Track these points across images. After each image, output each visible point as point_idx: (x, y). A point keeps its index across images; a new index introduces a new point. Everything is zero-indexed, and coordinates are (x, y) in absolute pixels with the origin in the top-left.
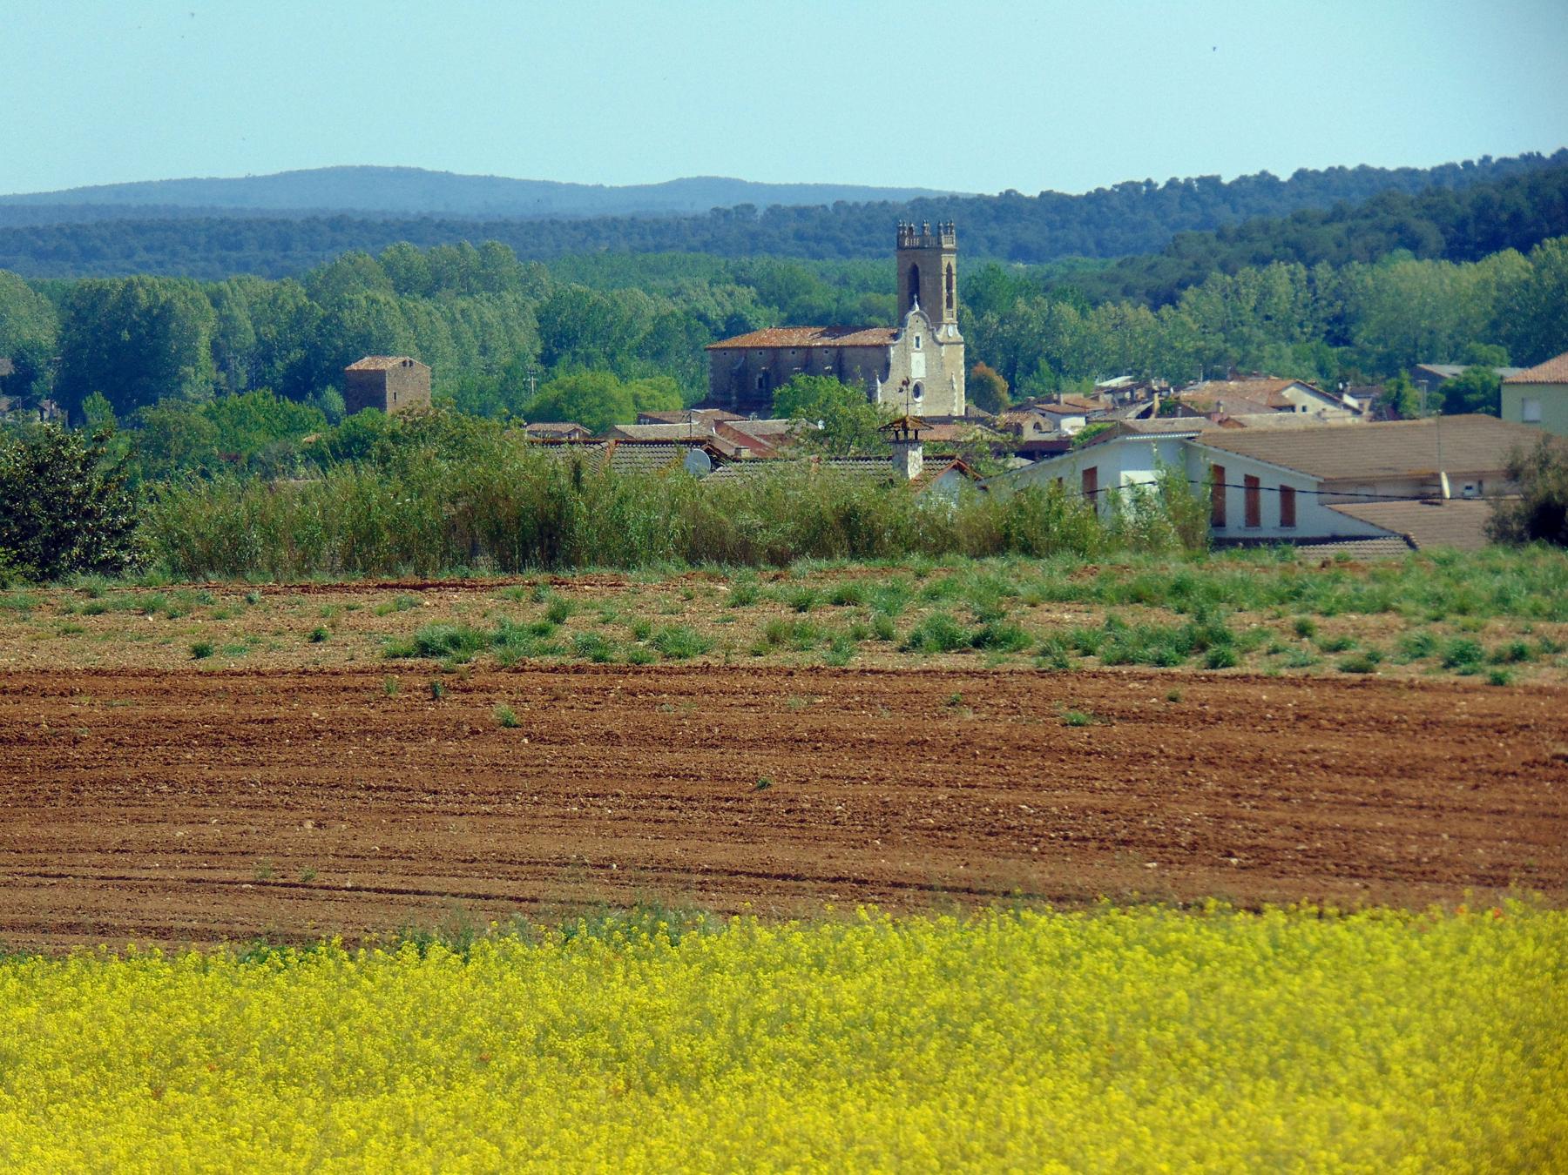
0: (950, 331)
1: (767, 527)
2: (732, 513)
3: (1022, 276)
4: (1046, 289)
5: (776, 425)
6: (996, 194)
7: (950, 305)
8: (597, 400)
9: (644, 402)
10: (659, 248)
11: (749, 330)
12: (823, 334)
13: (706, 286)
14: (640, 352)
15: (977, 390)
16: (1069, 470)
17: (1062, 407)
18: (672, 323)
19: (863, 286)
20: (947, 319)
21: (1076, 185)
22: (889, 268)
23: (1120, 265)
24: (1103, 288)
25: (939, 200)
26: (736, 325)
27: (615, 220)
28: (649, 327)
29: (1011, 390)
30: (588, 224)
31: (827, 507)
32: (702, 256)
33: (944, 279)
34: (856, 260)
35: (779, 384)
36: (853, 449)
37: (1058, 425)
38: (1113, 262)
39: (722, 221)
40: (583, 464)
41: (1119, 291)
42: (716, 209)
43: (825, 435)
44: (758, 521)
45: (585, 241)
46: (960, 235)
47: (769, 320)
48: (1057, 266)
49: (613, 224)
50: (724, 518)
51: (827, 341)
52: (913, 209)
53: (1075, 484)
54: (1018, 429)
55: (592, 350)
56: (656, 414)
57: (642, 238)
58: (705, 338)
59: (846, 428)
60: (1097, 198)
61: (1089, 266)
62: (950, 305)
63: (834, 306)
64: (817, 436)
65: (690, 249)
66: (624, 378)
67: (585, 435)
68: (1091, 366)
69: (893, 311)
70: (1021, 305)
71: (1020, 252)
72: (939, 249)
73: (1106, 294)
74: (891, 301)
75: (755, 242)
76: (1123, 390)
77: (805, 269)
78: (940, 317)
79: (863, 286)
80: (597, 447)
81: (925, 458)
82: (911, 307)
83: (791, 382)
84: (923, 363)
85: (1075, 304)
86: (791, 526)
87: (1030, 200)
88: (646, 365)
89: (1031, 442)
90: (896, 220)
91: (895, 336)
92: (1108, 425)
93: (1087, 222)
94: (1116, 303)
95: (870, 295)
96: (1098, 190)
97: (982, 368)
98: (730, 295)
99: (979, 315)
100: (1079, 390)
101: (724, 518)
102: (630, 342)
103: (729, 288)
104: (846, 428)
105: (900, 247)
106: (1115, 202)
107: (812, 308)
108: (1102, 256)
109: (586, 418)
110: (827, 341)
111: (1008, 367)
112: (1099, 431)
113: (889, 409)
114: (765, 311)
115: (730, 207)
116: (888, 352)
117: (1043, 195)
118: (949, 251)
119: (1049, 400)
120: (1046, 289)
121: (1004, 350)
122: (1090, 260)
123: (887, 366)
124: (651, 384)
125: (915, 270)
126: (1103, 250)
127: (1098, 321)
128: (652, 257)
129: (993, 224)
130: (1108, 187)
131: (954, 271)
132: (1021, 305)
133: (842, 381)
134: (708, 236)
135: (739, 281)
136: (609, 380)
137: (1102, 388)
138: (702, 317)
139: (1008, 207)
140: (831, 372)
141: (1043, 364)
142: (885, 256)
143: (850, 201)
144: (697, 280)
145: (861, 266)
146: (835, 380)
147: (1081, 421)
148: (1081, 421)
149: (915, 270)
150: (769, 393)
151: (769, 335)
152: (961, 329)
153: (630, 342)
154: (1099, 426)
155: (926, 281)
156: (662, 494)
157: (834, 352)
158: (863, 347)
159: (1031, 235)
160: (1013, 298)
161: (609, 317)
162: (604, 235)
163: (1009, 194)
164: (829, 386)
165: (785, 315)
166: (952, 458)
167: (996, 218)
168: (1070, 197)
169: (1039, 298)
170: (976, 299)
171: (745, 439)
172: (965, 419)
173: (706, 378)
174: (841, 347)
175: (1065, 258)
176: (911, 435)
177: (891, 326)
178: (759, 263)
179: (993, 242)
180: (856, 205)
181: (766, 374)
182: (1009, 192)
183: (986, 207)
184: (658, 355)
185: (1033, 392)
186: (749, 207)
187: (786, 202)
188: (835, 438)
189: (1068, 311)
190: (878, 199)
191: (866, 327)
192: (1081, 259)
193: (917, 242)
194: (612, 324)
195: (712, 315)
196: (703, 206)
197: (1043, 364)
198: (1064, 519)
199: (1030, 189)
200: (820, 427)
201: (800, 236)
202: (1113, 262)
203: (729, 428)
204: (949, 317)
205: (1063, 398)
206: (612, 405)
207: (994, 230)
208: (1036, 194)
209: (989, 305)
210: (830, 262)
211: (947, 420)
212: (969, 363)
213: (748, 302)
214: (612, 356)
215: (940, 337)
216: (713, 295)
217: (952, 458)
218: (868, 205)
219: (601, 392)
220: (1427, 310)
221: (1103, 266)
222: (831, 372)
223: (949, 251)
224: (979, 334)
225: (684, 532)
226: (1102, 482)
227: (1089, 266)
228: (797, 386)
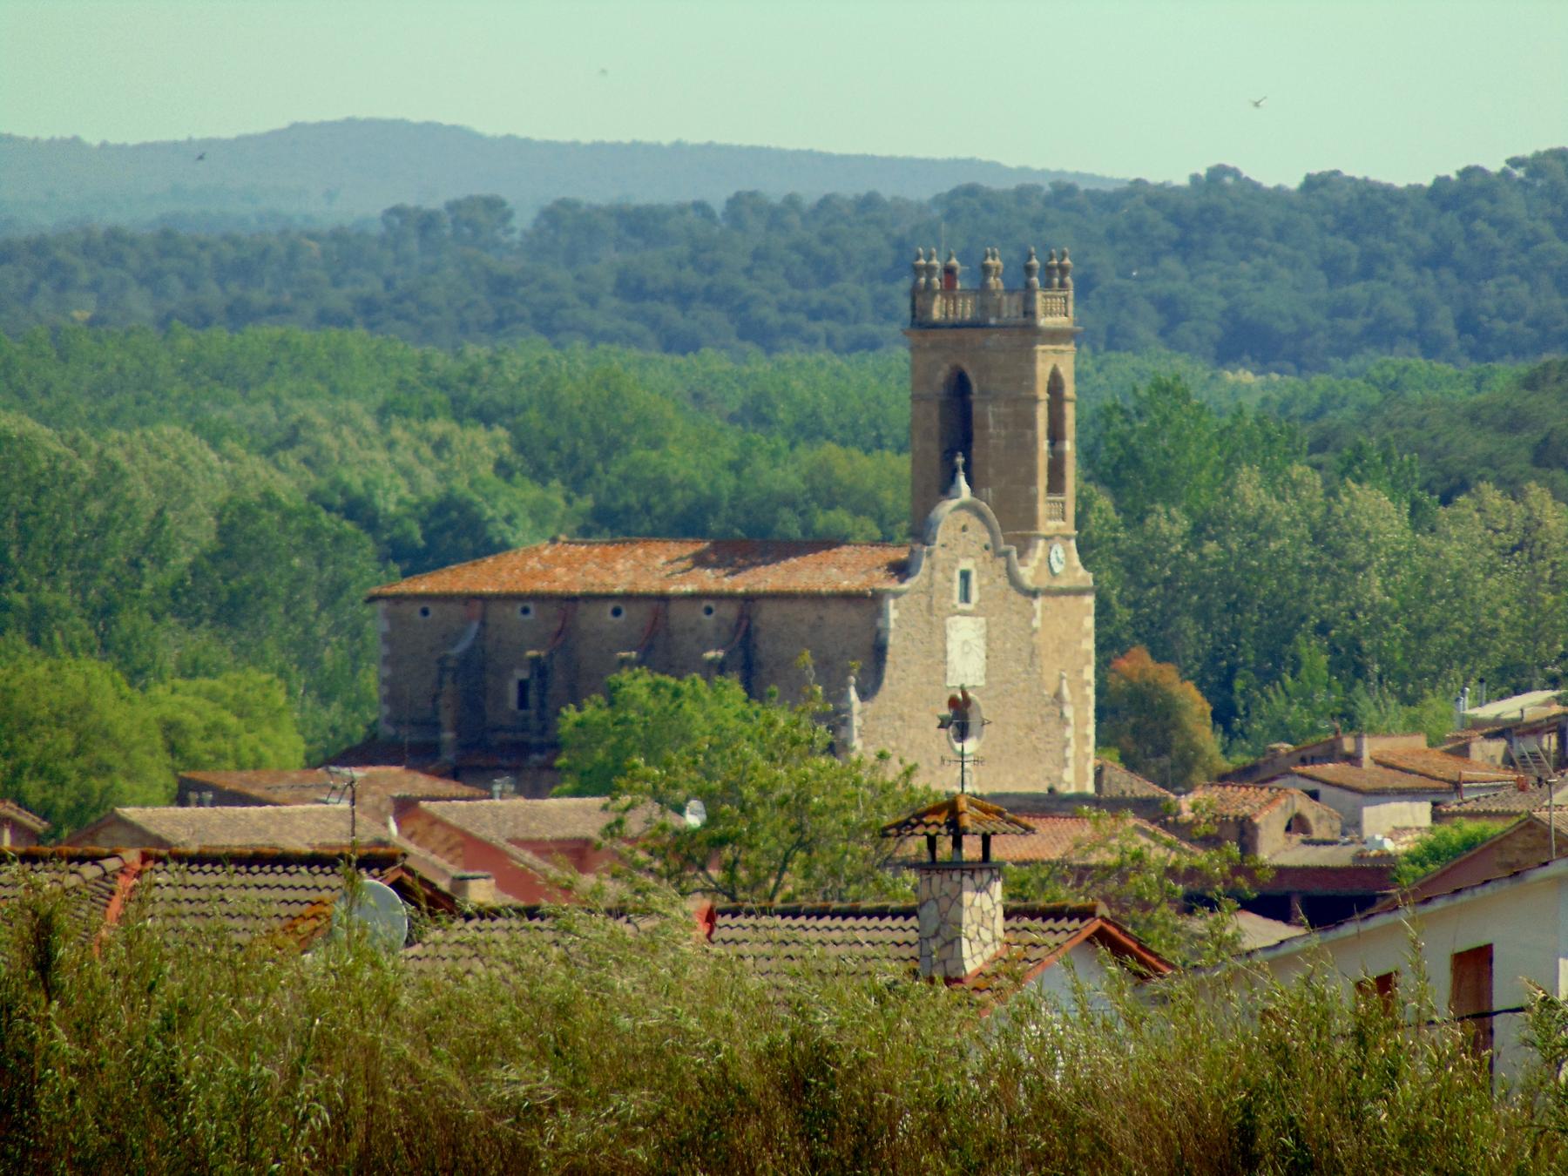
0: (1056, 557)
1: (571, 1102)
2: (473, 1059)
3: (1251, 403)
4: (1319, 446)
5: (571, 814)
6: (1182, 180)
7: (1056, 485)
8: (68, 742)
9: (197, 746)
10: (239, 315)
11: (488, 547)
12: (700, 561)
13: (369, 424)
14: (180, 603)
15: (1131, 723)
16: (1413, 948)
17: (1367, 773)
18: (269, 520)
19: (809, 429)
20: (1048, 526)
21: (1407, 159)
22: (889, 381)
23: (1531, 383)
24: (1480, 444)
25: (1023, 194)
26: (455, 531)
27: (114, 235)
28: (205, 534)
29: (1223, 716)
30: (39, 247)
31: (743, 1051)
32: (357, 340)
33: (1042, 413)
34: (790, 357)
35: (576, 697)
36: (792, 882)
37: (1353, 824)
38: (1505, 374)
39: (413, 245)
40: (63, 920)
41: (1525, 453)
42: (397, 211)
43: (714, 841)
44: (547, 1083)
45: (33, 289)
46: (1085, 287)
47: (540, 515)
48: (1350, 384)
49: (108, 247)
50: (454, 1079)
51: (710, 580)
52: (952, 215)
53: (1430, 989)
54: (1245, 832)
55: (46, 596)
56: (232, 781)
57: (191, 286)
58: (364, 567)
59: (772, 832)
60: (1463, 195)
61: (1441, 384)
62: (1056, 485)
63: (727, 482)
64: (683, 856)
65: (325, 318)
66: (136, 675)
67: (32, 835)
68: (1445, 660)
69: (896, 499)
70: (1251, 489)
71: (1244, 340)
72: (1027, 331)
73: (1489, 461)
74: (889, 472)
75: (506, 304)
76: (1536, 729)
77: (650, 379)
78: (1032, 521)
79: (809, 429)
80: (90, 871)
81: (1008, 915)
82: (946, 488)
83: (612, 696)
84: (979, 646)
85: (1396, 487)
86: (635, 1103)
87: (1278, 195)
88: (201, 641)
89: (1282, 871)
90: (900, 244)
91: (901, 570)
92: (1497, 827)
93: (1438, 259)
94: (1513, 489)
95: (830, 450)
96: (1467, 173)
97: (1138, 663)
98: (441, 446)
99: (1135, 517)
100: (1414, 725)
101: (454, 1079)
102: (153, 580)
103: (438, 427)
104: (772, 832)
105: (920, 322)
106: (1515, 206)
107: (661, 486)
108: (1474, 354)
109: (32, 788)
110: (710, 580)
111: (1211, 658)
112: (1469, 844)
113: (892, 772)
114: (530, 492)
115: (435, 203)
116: (880, 612)
117: (1312, 184)
118: (1055, 336)
119: (1332, 753)
120: (1319, 446)
121: (1202, 614)
122: (1444, 369)
123: (878, 652)
124: (212, 696)
125: (960, 386)
126: (1477, 338)
127: (1466, 534)
128: (219, 338)
129: (1171, 263)
130: (1495, 165)
131: (1070, 390)
132: (1251, 489)
133: (753, 690)
134: (373, 286)
135: (462, 411)
136: (93, 678)
137: (1477, 724)
138: (358, 510)
139: (1212, 216)
140: (721, 668)
141: (1314, 655)
142: (873, 344)
143: (774, 189)
144: (341, 405)
145: (808, 375)
146: (734, 689)
147: (1421, 813)
148: (1421, 813)
149: (960, 386)
150: (547, 720)
151: (546, 561)
152: (1087, 549)
153: (153, 580)
154: (1471, 827)
155: (990, 416)
156: (284, 1003)
157: (729, 611)
158: (815, 598)
159: (1281, 297)
160: (1228, 467)
161: (95, 508)
162: (84, 277)
163: (1138, 182)
164: (717, 706)
165: (586, 503)
166: (1085, 914)
167: (1183, 248)
168: (1388, 192)
169: (1297, 470)
170: (1126, 469)
171: (478, 852)
172: (1106, 803)
173: (370, 680)
174: (750, 599)
175: (1388, 363)
176: (971, 849)
177: (885, 540)
178: (522, 358)
179: (1171, 312)
180: (792, 202)
181: (540, 669)
182: (1218, 172)
183: (1151, 214)
184: (231, 612)
185: (1282, 731)
186: (492, 204)
187: (598, 193)
188: (724, 862)
189: (1376, 509)
190: (850, 188)
191: (826, 542)
192: (1419, 363)
193: (966, 309)
194: (106, 522)
195: (388, 504)
196: (362, 203)
197: (1314, 655)
198: (1406, 1090)
199: (1278, 167)
200: (693, 819)
201: (632, 289)
202: (1505, 374)
203: (434, 821)
204: (1054, 519)
205: (1371, 747)
206: (110, 756)
207: (1174, 276)
208: (1294, 182)
209: (1165, 487)
210: (714, 361)
211: (1052, 805)
212: (1108, 646)
213: (486, 471)
214: (105, 612)
215: (1028, 573)
216: (391, 445)
217: (1085, 914)
218: (826, 203)
219: (74, 715)
220: (1264, 523)
221: (1479, 382)
222: (721, 668)
223: (1055, 336)
224: (1132, 566)
225: (339, 1114)
226: (1506, 988)
227: (1441, 384)
228: (629, 701)
